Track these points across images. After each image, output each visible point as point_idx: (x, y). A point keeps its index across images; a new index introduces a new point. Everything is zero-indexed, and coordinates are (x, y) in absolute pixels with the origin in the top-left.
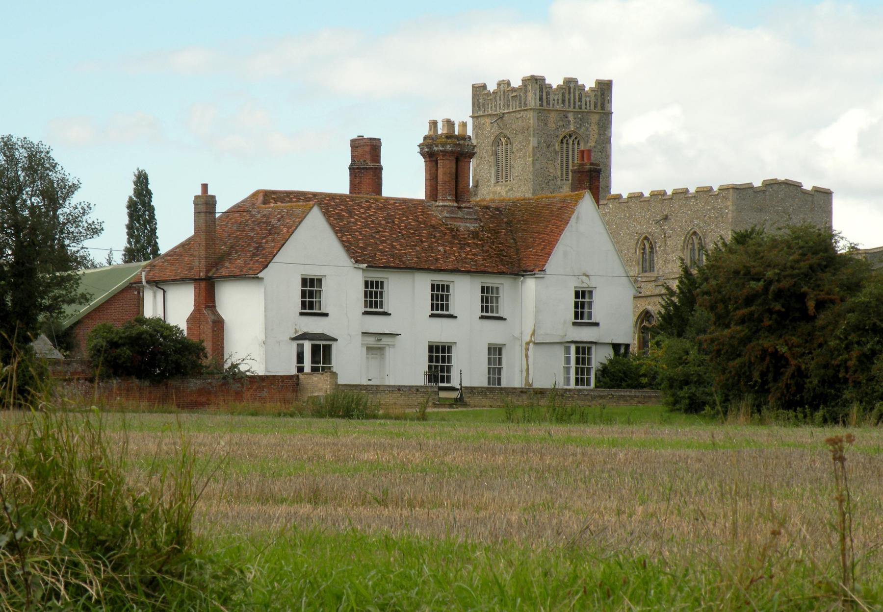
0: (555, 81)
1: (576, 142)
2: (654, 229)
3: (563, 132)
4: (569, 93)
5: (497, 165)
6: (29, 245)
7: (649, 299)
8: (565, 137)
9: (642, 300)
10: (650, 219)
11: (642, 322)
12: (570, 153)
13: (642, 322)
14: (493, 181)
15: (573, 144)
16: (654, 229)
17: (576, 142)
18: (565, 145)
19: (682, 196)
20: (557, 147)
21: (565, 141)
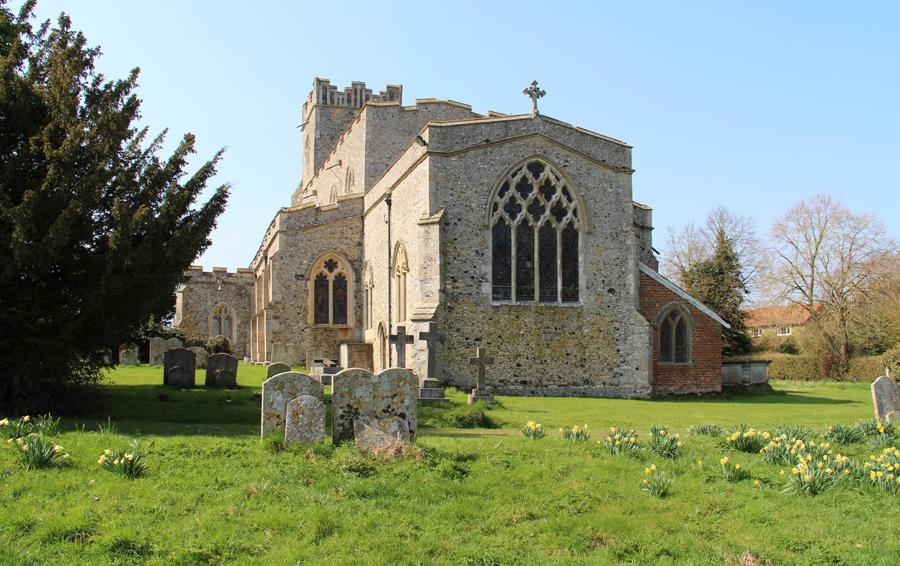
4: (356, 93)
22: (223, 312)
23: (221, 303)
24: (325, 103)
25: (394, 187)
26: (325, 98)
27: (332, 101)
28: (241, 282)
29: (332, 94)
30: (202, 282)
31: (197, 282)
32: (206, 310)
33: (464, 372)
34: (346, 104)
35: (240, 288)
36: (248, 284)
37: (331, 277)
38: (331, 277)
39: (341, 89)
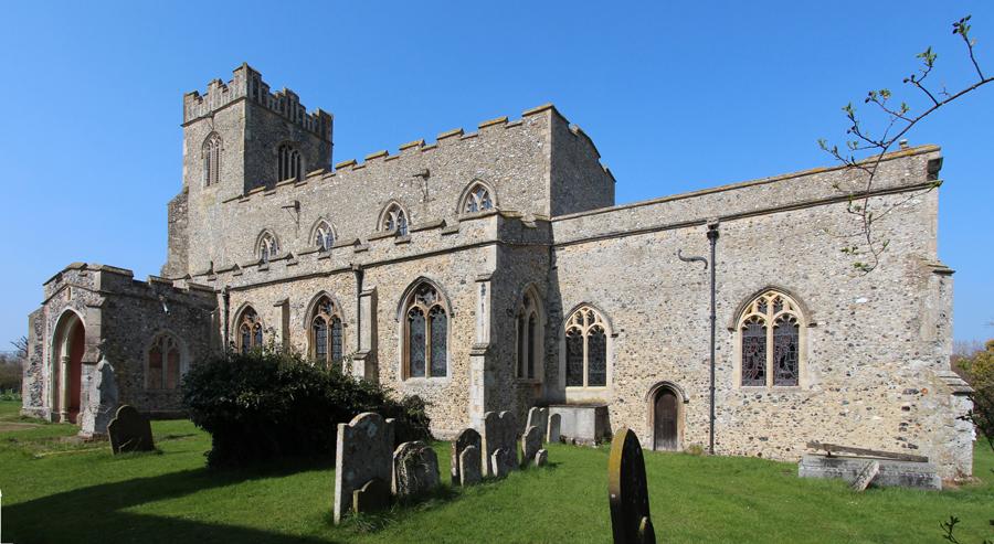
4: (289, 104)
11: (412, 301)
12: (290, 163)
14: (203, 183)
15: (293, 157)
20: (275, 151)
21: (284, 150)
22: (165, 344)
23: (164, 330)
24: (256, 99)
25: (64, 272)
26: (255, 92)
27: (264, 102)
28: (194, 303)
29: (264, 92)
30: (133, 296)
31: (124, 295)
32: (138, 340)
33: (502, 474)
34: (279, 112)
35: (193, 311)
36: (206, 307)
37: (770, 319)
38: (770, 319)
39: (273, 91)
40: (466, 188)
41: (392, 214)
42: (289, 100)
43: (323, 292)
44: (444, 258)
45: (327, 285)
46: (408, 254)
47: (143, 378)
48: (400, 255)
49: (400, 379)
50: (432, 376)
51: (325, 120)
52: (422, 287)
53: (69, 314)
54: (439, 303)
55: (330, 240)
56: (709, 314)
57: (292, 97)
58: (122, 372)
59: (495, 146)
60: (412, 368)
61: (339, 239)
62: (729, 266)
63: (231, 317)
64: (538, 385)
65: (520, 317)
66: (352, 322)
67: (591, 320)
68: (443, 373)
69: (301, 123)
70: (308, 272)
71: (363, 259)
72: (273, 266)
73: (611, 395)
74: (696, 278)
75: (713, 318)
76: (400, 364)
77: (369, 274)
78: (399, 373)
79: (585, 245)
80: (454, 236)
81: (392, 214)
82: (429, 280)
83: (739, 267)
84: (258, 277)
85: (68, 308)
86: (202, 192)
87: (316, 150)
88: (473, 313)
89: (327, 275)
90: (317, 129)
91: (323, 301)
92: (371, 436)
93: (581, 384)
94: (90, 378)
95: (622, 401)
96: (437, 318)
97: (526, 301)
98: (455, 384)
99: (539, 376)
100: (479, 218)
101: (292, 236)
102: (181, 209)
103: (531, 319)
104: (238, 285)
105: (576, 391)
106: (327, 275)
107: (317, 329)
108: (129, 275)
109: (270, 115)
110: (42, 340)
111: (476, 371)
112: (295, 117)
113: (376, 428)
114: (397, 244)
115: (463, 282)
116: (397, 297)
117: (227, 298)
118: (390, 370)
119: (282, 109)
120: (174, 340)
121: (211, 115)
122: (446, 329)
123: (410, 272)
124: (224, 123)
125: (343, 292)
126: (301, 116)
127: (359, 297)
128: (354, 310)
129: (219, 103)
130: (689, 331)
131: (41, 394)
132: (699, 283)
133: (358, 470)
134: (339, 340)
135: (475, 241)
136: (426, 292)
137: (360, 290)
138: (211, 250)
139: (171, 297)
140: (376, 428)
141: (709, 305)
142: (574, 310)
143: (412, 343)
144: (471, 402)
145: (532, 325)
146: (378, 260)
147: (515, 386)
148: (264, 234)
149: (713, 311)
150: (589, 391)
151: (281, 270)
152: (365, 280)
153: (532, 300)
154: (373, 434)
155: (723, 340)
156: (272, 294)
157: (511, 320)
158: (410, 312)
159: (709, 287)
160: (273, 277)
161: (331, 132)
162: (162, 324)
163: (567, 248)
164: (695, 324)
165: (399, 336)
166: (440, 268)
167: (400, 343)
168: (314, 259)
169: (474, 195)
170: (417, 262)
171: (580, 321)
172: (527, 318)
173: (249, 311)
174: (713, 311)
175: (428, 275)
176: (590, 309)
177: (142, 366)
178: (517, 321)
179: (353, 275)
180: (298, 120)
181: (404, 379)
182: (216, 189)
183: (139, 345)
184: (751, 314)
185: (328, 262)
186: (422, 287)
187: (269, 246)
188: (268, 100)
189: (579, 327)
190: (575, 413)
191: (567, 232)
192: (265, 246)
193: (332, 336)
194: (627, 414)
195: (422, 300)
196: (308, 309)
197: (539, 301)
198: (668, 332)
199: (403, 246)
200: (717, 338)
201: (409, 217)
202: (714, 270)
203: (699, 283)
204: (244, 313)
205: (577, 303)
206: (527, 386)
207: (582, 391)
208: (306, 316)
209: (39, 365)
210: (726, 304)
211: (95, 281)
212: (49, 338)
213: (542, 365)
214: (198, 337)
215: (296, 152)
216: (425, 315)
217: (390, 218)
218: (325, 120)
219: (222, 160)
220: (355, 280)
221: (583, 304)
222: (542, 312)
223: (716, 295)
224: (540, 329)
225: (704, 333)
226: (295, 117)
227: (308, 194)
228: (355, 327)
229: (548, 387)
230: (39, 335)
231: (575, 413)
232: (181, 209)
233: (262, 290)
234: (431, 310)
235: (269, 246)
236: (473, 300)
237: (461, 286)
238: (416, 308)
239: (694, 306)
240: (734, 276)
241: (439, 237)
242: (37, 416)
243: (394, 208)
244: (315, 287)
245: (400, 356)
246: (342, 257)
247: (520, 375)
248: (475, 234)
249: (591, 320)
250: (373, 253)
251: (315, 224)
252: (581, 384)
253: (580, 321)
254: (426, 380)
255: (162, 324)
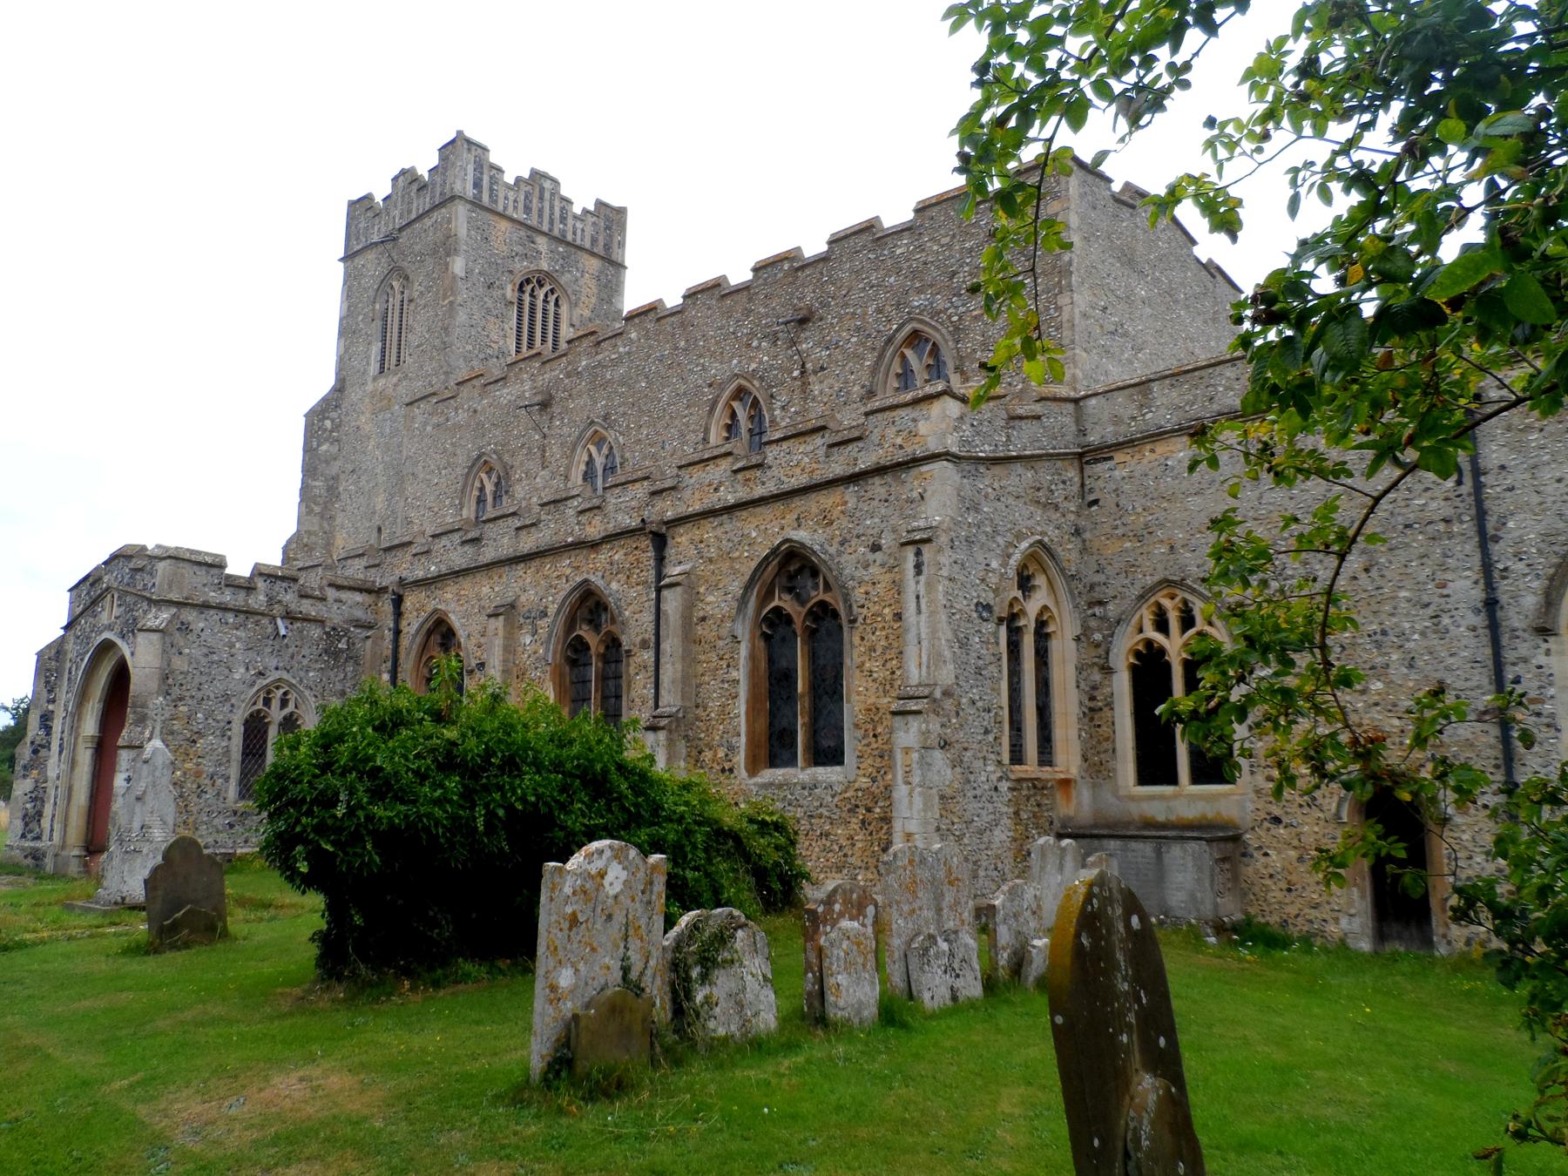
0: (514, 167)
1: (552, 299)
2: (763, 357)
3: (521, 267)
4: (541, 198)
5: (384, 341)
6: (1541, 966)
7: (798, 504)
8: (528, 281)
9: (766, 512)
10: (752, 335)
11: (768, 595)
12: (539, 316)
13: (768, 595)
14: (374, 368)
15: (546, 301)
16: (763, 357)
17: (552, 299)
18: (527, 298)
19: (865, 237)
20: (510, 293)
21: (528, 288)
22: (275, 704)
29: (494, 181)
30: (223, 608)
32: (226, 697)
40: (890, 340)
41: (736, 404)
42: (542, 190)
43: (586, 581)
44: (827, 499)
45: (596, 569)
46: (759, 491)
47: (227, 779)
48: (743, 494)
49: (744, 774)
50: (817, 763)
51: (610, 219)
52: (793, 565)
53: (107, 647)
54: (827, 598)
55: (609, 469)
56: (1478, 594)
57: (547, 185)
58: (188, 765)
59: (949, 246)
60: (774, 746)
61: (628, 469)
62: (1518, 477)
63: (405, 642)
64: (1066, 783)
65: (1011, 621)
66: (644, 645)
67: (1187, 621)
68: (832, 756)
69: (563, 233)
70: (557, 540)
71: (669, 509)
72: (491, 531)
73: (1250, 806)
74: (1439, 508)
75: (1491, 604)
76: (743, 739)
77: (682, 541)
78: (741, 758)
79: (1161, 448)
80: (852, 448)
81: (736, 404)
82: (803, 545)
83: (1547, 474)
84: (459, 557)
85: (107, 635)
86: (370, 387)
87: (593, 284)
88: (898, 617)
89: (594, 545)
90: (594, 241)
91: (589, 605)
92: (612, 892)
93: (1172, 779)
94: (128, 780)
95: (1277, 820)
96: (823, 630)
97: (1025, 583)
98: (864, 782)
99: (1068, 759)
100: (906, 405)
101: (533, 465)
102: (328, 423)
103: (1041, 624)
104: (420, 574)
105: (1162, 797)
106: (594, 545)
107: (573, 663)
108: (216, 565)
109: (504, 225)
110: (53, 701)
111: (907, 750)
112: (551, 222)
113: (624, 875)
114: (735, 472)
115: (876, 548)
116: (736, 587)
117: (398, 601)
118: (721, 754)
119: (527, 209)
120: (292, 697)
121: (391, 239)
122: (841, 654)
123: (764, 533)
124: (417, 248)
125: (622, 581)
126: (563, 219)
127: (659, 590)
128: (648, 617)
129: (410, 212)
130: (1433, 640)
131: (40, 814)
132: (1447, 521)
133: (581, 966)
134: (618, 687)
135: (900, 457)
136: (800, 571)
137: (660, 576)
138: (380, 502)
139: (293, 607)
140: (624, 875)
141: (1474, 573)
142: (1142, 598)
143: (775, 685)
144: (897, 825)
145: (1042, 636)
146: (697, 507)
147: (1004, 786)
148: (481, 463)
149: (1490, 586)
150: (1193, 798)
151: (506, 540)
152: (671, 552)
153: (1040, 580)
154: (618, 888)
155: (1525, 660)
156: (486, 590)
157: (991, 627)
158: (765, 618)
159: (1467, 526)
160: (489, 554)
161: (622, 244)
162: (273, 662)
163: (1119, 457)
164: (1446, 621)
165: (741, 674)
166: (826, 520)
167: (743, 691)
168: (571, 512)
169: (909, 353)
170: (779, 507)
171: (1162, 625)
172: (1028, 622)
173: (441, 633)
174: (1490, 586)
175: (802, 535)
176: (1181, 595)
177: (227, 751)
178: (1003, 630)
179: (646, 543)
180: (558, 226)
181: (753, 770)
182: (395, 379)
183: (227, 708)
184: (1141, 636)
185: (597, 520)
186: (793, 565)
187: (489, 488)
188: (501, 195)
189: (1158, 637)
190: (1159, 854)
191: (1117, 420)
192: (482, 489)
193: (603, 678)
194: (1293, 854)
195: (790, 590)
196: (554, 621)
197: (1060, 583)
198: (1379, 645)
199: (748, 474)
200: (1509, 655)
201: (771, 410)
202: (1478, 487)
203: (1447, 521)
204: (429, 633)
205: (1150, 581)
206: (1037, 785)
207: (1175, 796)
208: (550, 636)
209: (43, 752)
210: (1521, 567)
211: (157, 581)
212: (66, 696)
213: (1073, 733)
214: (339, 687)
215: (552, 291)
216: (798, 625)
217: (733, 415)
218: (610, 219)
219: (409, 320)
220: (651, 554)
221: (1166, 583)
222: (1067, 606)
223: (1495, 548)
224: (1064, 652)
225: (1473, 642)
226: (551, 222)
227: (568, 375)
228: (648, 656)
229: (1094, 786)
230: (50, 692)
231: (1159, 854)
232: (328, 423)
233: (466, 584)
234: (810, 612)
235: (489, 488)
236: (898, 587)
237: (871, 557)
238: (777, 610)
239: (1440, 576)
240: (1535, 499)
241: (821, 452)
242: (29, 861)
243: (740, 393)
244: (562, 577)
245: (743, 719)
246: (624, 509)
247: (1017, 756)
248: (899, 441)
249: (1187, 621)
250: (687, 494)
251: (580, 437)
252: (1172, 779)
253: (1162, 625)
254: (801, 774)
255: (273, 662)
